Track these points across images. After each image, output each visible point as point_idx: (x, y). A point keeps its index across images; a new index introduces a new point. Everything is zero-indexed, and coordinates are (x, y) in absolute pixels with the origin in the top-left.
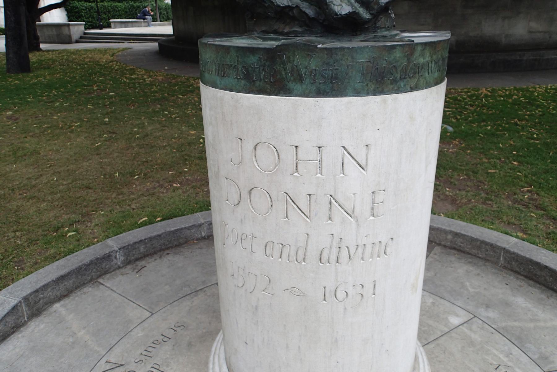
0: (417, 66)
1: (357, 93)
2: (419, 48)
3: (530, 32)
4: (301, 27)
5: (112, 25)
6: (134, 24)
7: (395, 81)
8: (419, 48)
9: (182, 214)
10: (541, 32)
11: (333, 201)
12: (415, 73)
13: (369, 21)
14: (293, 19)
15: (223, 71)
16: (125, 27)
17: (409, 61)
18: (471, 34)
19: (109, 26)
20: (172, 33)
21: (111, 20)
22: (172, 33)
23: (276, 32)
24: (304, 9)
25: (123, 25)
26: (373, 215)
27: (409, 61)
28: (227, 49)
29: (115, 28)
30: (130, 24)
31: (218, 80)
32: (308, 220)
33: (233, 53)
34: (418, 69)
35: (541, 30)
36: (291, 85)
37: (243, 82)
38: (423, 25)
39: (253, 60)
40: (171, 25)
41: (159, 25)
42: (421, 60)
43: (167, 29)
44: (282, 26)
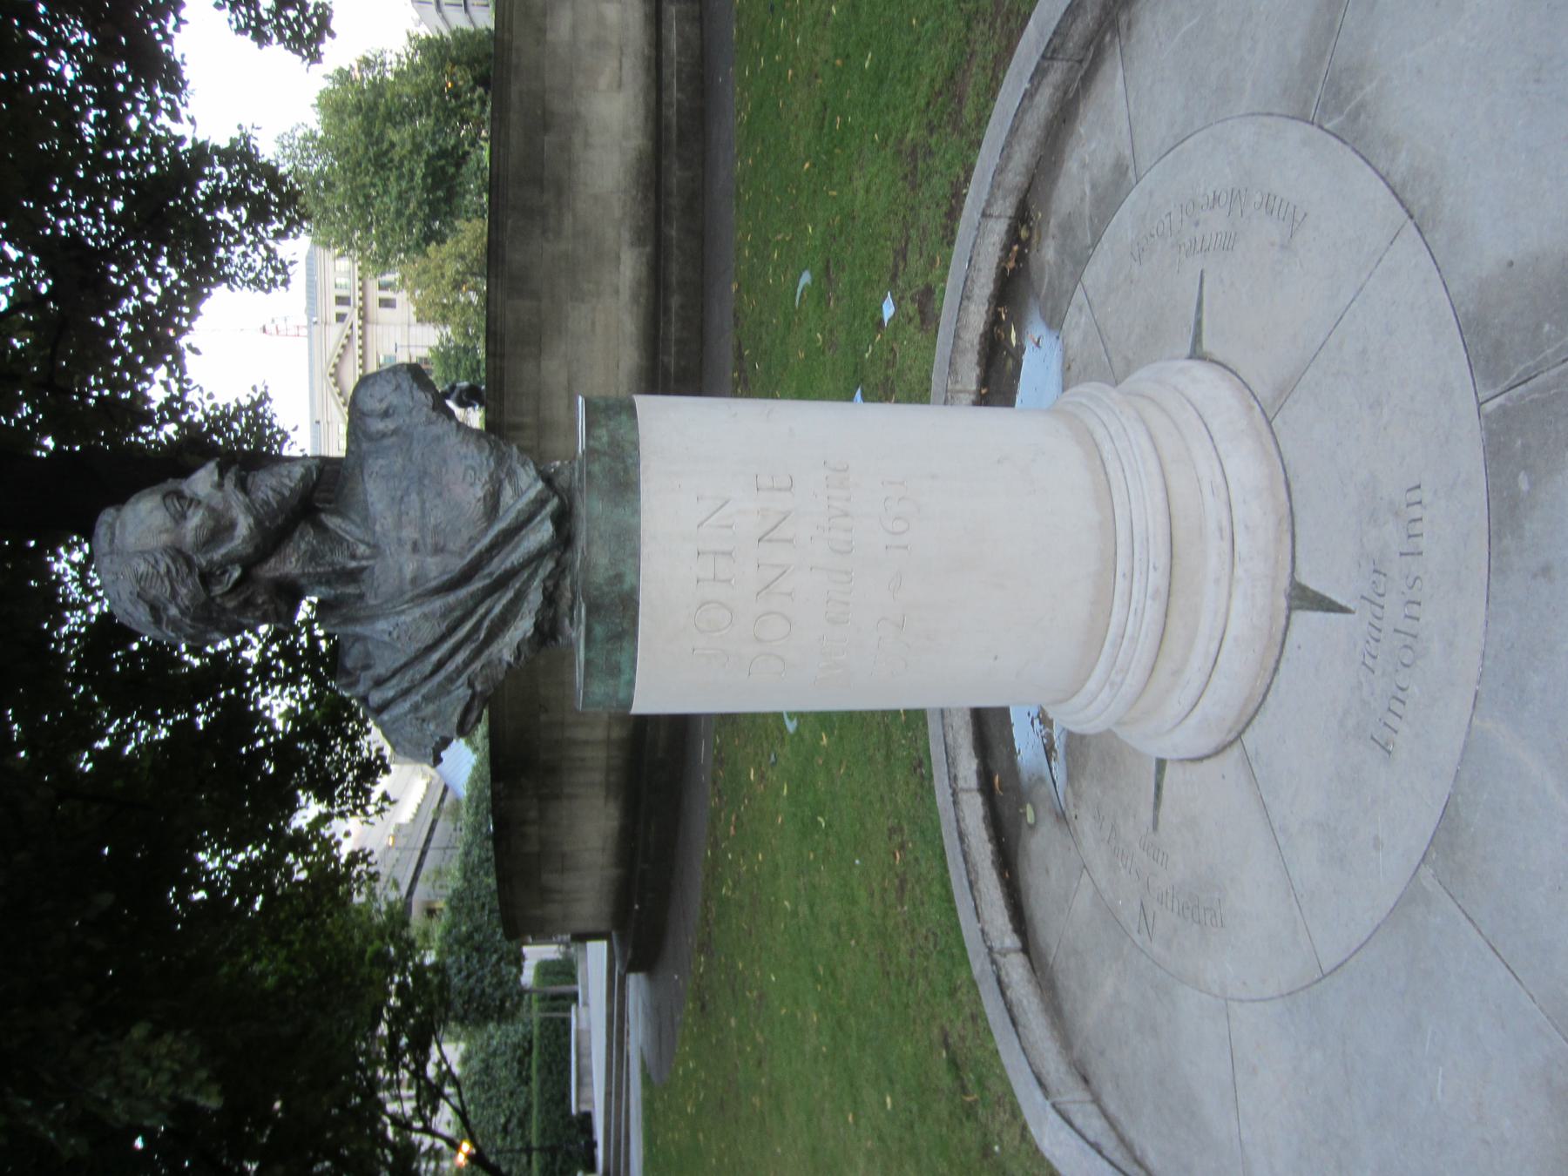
0: (610, 444)
2: (591, 443)
3: (620, 85)
4: (565, 577)
5: (584, 1108)
6: (583, 1051)
7: (626, 470)
8: (591, 443)
9: (370, 437)
10: (621, 62)
11: (766, 538)
12: (618, 446)
13: (561, 499)
14: (557, 586)
15: (614, 671)
16: (590, 1073)
17: (605, 454)
18: (617, 213)
19: (587, 1118)
20: (605, 943)
21: (574, 1111)
22: (605, 943)
23: (571, 609)
24: (547, 573)
25: (586, 1080)
27: (605, 454)
28: (588, 662)
29: (591, 1101)
30: (584, 1061)
31: (625, 677)
32: (792, 568)
33: (592, 655)
34: (615, 443)
35: (615, 64)
36: (626, 586)
37: (625, 644)
38: (593, 324)
39: (599, 630)
40: (585, 949)
41: (586, 987)
42: (605, 439)
43: (596, 955)
44: (564, 600)
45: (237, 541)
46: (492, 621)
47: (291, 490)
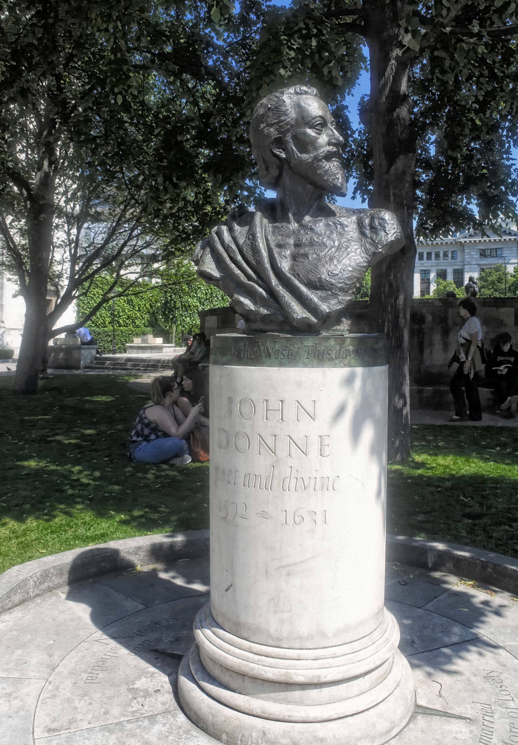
1: (305, 365)
7: (331, 359)
26: (321, 455)
45: (299, 155)
46: (253, 287)
47: (328, 180)
